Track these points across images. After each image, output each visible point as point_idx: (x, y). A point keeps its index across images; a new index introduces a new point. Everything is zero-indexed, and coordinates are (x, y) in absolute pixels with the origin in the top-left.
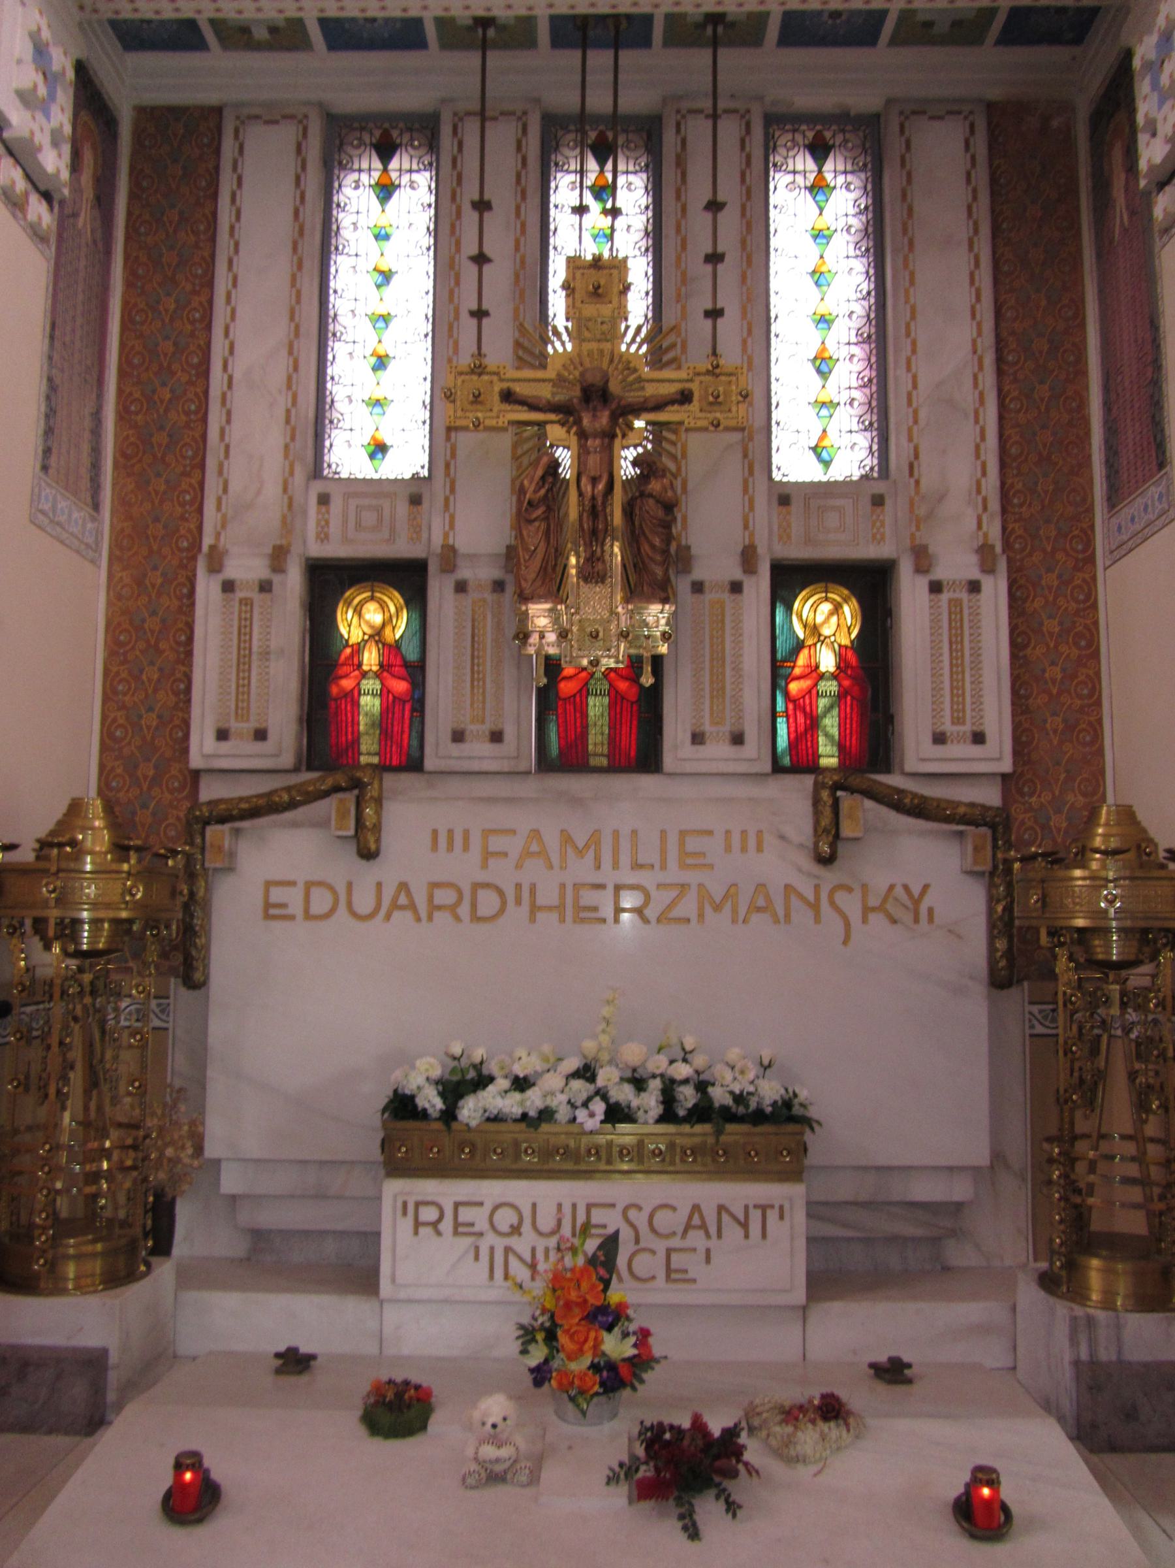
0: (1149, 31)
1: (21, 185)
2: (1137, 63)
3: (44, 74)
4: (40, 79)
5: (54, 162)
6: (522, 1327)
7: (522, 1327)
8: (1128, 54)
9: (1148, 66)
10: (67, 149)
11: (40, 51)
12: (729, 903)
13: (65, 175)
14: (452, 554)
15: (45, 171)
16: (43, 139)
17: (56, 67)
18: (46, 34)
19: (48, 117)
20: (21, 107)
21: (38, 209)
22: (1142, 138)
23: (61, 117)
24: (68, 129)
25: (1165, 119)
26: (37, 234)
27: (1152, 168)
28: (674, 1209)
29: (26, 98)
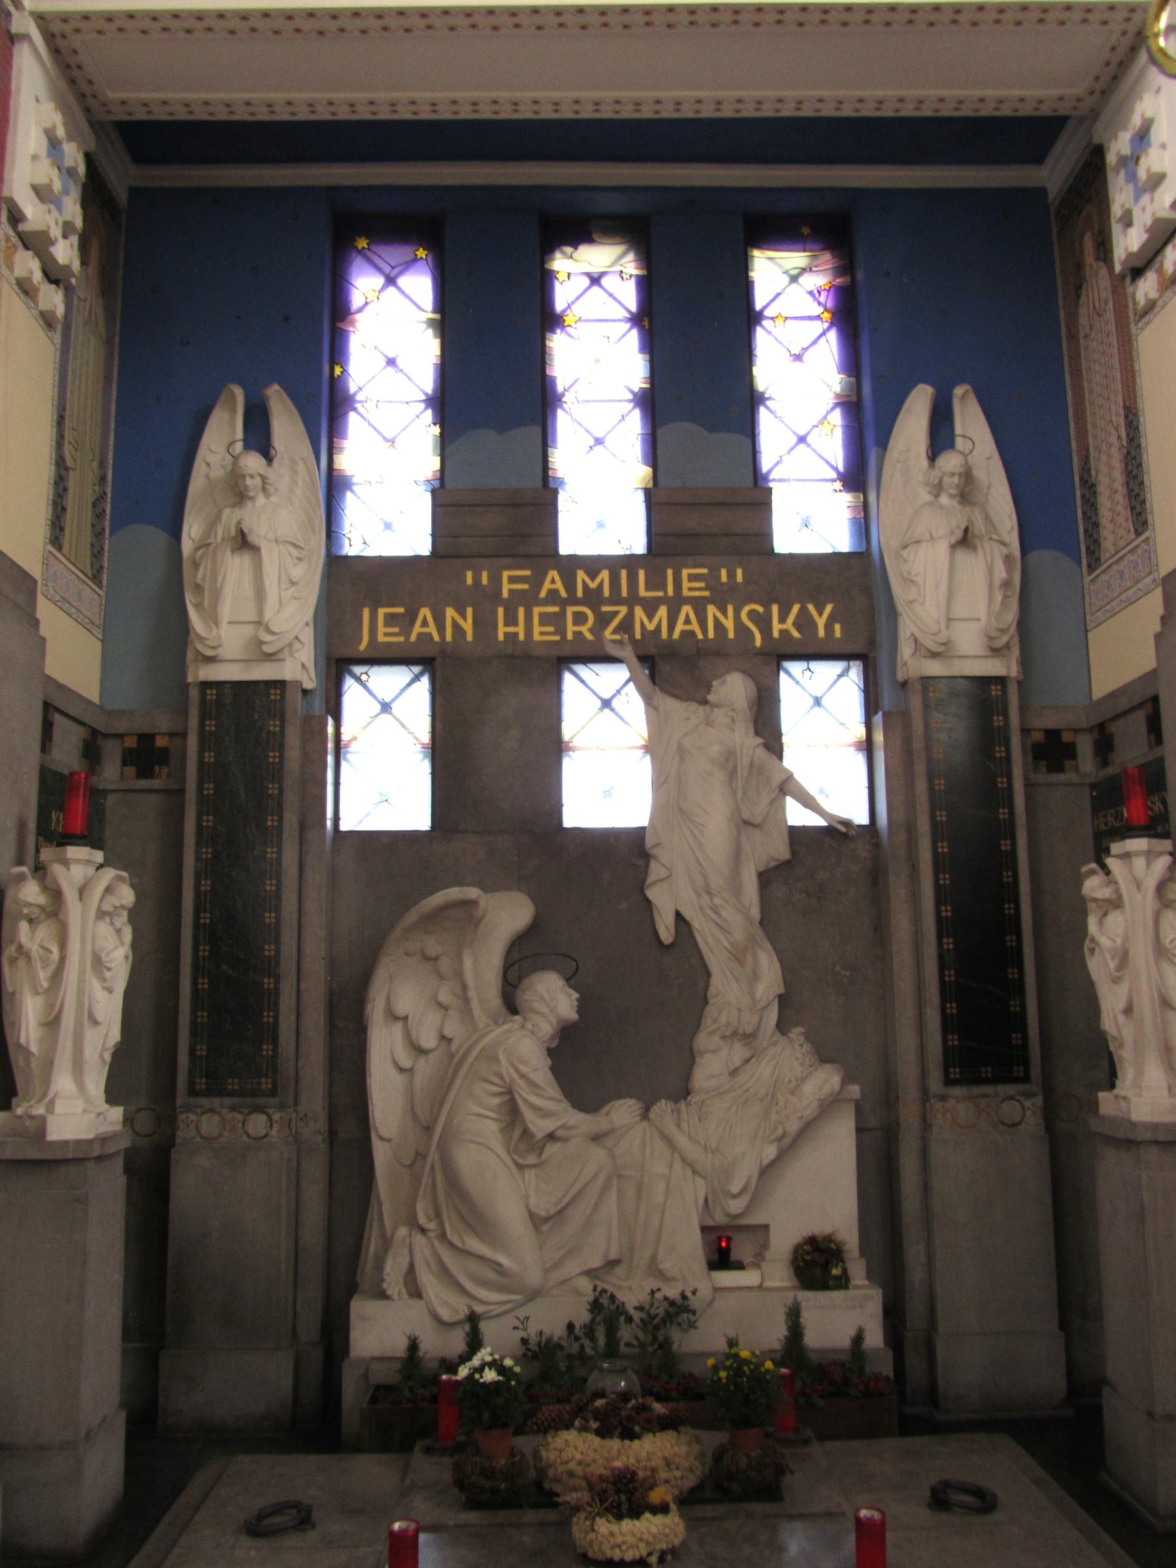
0: (1124, 128)
1: (38, 276)
2: (1111, 159)
3: (59, 169)
4: (55, 173)
5: (65, 252)
6: (695, 1328)
7: (695, 1328)
8: (1098, 153)
9: (1123, 161)
10: (75, 239)
11: (54, 143)
12: (614, 1192)
13: (76, 266)
14: (521, 1161)
15: (56, 262)
16: (56, 232)
17: (68, 162)
18: (61, 132)
19: (59, 209)
20: (36, 200)
21: (53, 299)
22: (1116, 229)
23: (73, 210)
24: (79, 223)
25: (1144, 209)
26: (48, 320)
27: (1130, 255)
28: (979, 620)
29: (42, 193)
